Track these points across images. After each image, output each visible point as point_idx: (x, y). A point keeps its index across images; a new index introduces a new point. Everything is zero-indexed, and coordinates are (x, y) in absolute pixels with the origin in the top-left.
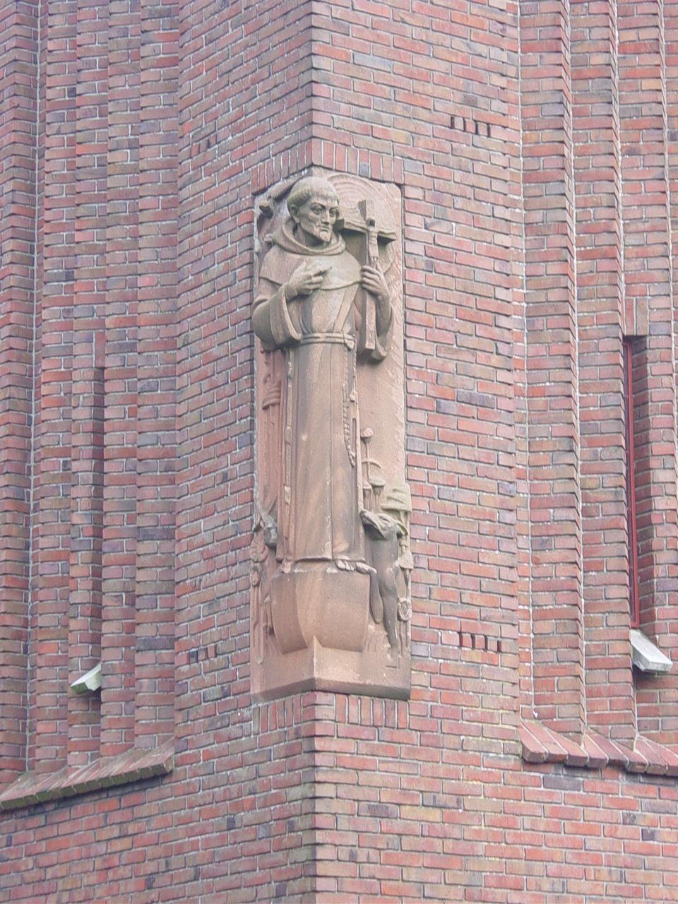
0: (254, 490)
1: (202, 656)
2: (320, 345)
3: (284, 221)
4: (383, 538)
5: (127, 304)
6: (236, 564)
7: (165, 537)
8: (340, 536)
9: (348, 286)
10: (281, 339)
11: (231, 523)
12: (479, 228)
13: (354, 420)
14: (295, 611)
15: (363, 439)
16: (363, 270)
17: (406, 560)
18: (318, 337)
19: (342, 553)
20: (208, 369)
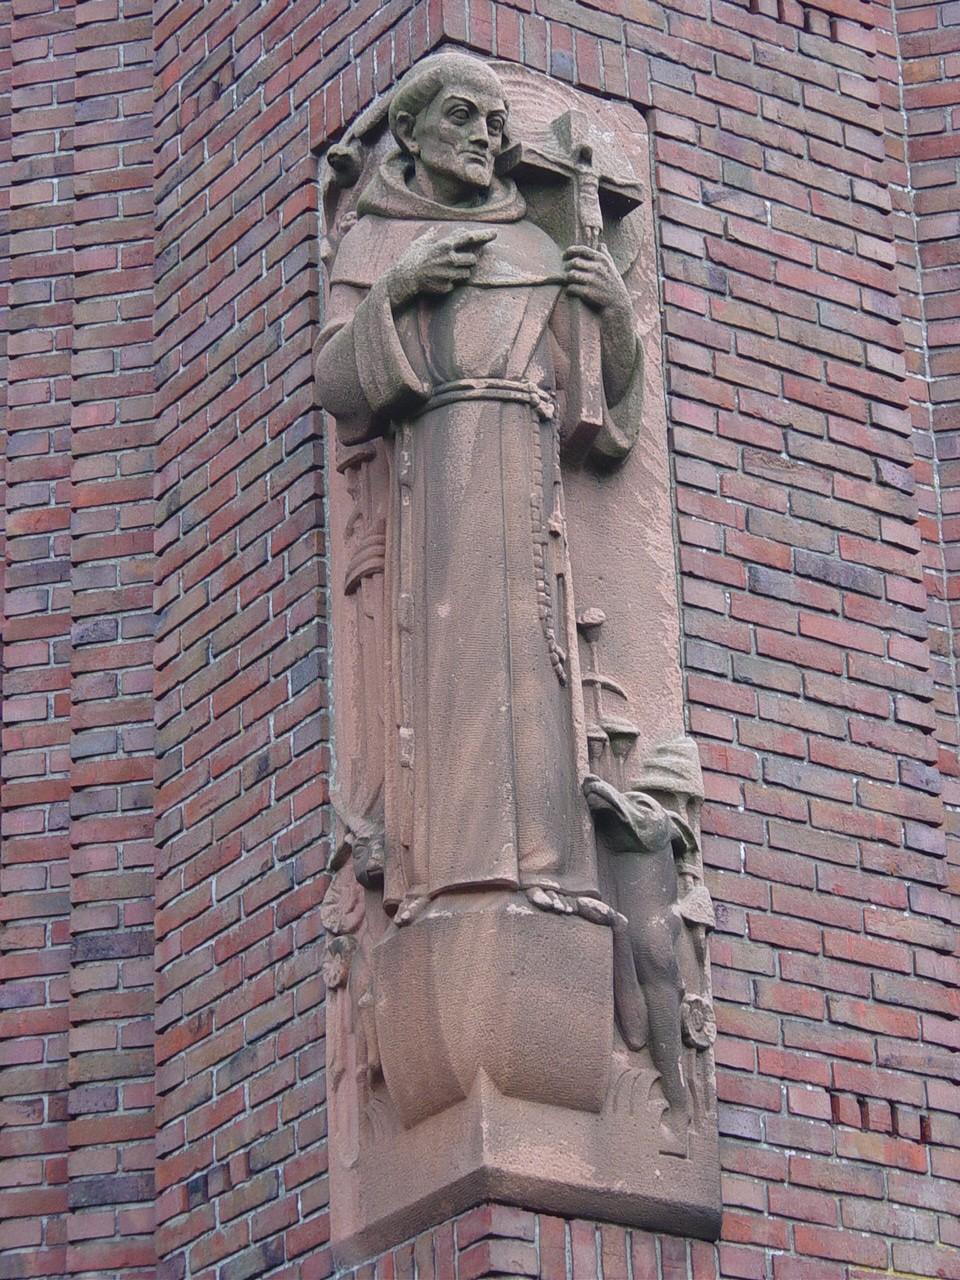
0: (331, 779)
1: (215, 1186)
2: (474, 405)
3: (384, 160)
4: (639, 847)
5: (53, 484)
6: (291, 953)
7: (135, 951)
8: (535, 831)
9: (535, 285)
10: (381, 396)
11: (278, 866)
12: (823, 218)
13: (560, 576)
14: (432, 1012)
15: (586, 631)
16: (569, 256)
17: (695, 902)
18: (470, 388)
19: (542, 871)
20: (224, 547)
